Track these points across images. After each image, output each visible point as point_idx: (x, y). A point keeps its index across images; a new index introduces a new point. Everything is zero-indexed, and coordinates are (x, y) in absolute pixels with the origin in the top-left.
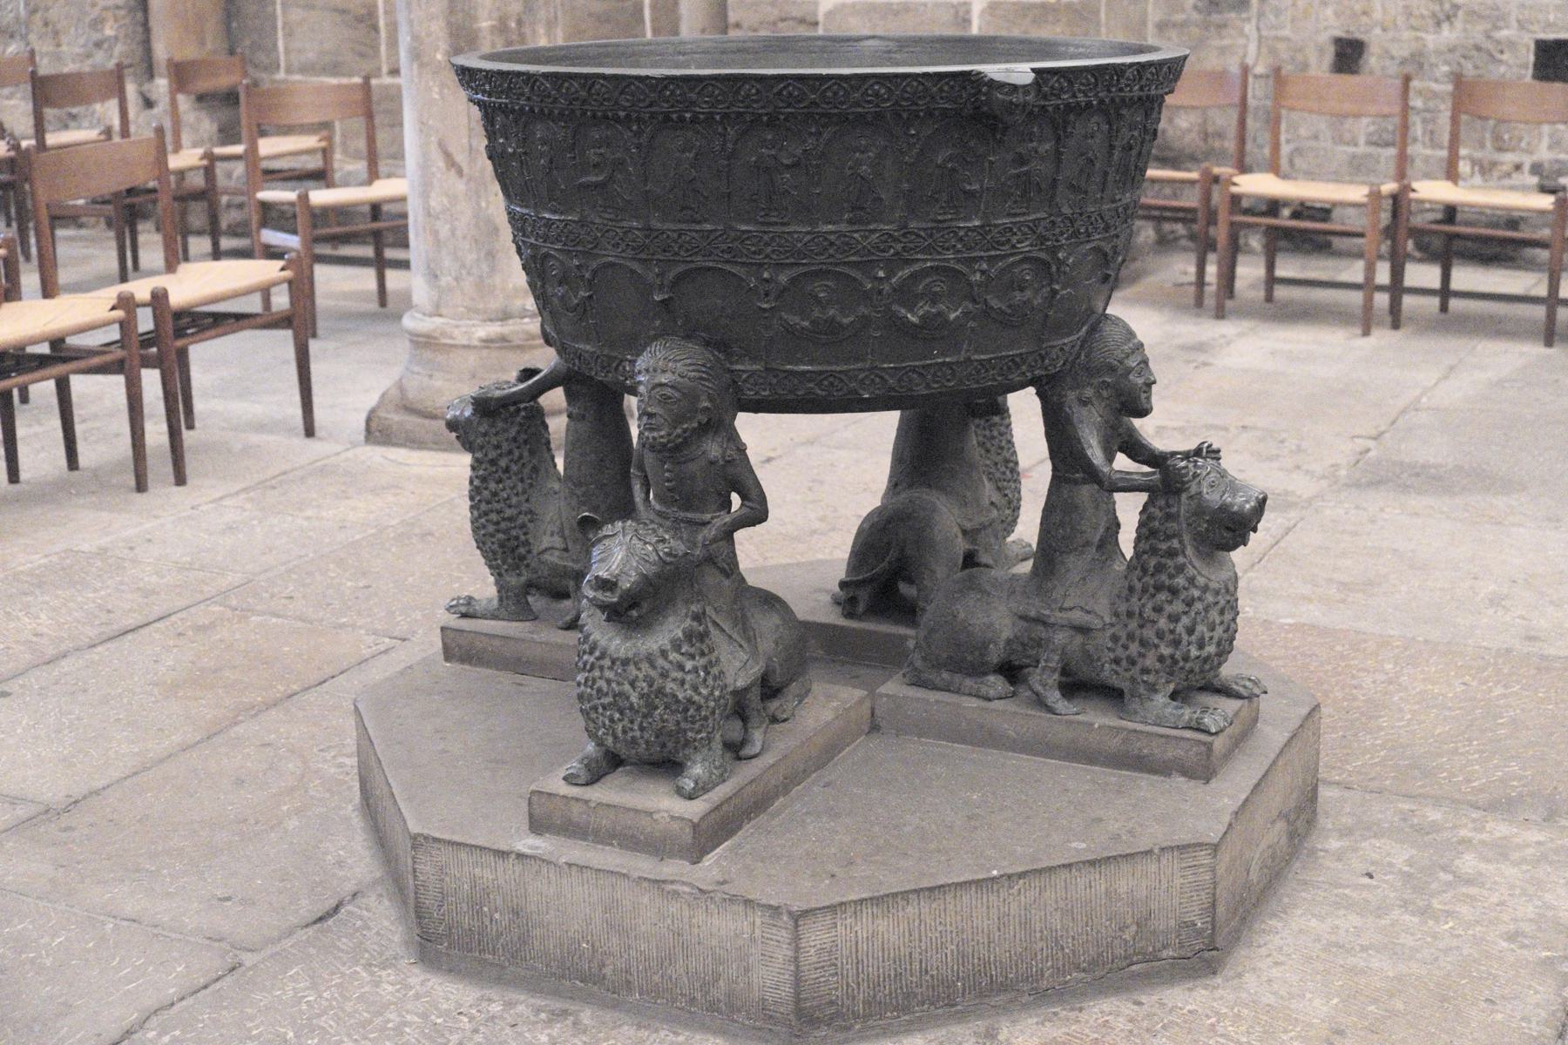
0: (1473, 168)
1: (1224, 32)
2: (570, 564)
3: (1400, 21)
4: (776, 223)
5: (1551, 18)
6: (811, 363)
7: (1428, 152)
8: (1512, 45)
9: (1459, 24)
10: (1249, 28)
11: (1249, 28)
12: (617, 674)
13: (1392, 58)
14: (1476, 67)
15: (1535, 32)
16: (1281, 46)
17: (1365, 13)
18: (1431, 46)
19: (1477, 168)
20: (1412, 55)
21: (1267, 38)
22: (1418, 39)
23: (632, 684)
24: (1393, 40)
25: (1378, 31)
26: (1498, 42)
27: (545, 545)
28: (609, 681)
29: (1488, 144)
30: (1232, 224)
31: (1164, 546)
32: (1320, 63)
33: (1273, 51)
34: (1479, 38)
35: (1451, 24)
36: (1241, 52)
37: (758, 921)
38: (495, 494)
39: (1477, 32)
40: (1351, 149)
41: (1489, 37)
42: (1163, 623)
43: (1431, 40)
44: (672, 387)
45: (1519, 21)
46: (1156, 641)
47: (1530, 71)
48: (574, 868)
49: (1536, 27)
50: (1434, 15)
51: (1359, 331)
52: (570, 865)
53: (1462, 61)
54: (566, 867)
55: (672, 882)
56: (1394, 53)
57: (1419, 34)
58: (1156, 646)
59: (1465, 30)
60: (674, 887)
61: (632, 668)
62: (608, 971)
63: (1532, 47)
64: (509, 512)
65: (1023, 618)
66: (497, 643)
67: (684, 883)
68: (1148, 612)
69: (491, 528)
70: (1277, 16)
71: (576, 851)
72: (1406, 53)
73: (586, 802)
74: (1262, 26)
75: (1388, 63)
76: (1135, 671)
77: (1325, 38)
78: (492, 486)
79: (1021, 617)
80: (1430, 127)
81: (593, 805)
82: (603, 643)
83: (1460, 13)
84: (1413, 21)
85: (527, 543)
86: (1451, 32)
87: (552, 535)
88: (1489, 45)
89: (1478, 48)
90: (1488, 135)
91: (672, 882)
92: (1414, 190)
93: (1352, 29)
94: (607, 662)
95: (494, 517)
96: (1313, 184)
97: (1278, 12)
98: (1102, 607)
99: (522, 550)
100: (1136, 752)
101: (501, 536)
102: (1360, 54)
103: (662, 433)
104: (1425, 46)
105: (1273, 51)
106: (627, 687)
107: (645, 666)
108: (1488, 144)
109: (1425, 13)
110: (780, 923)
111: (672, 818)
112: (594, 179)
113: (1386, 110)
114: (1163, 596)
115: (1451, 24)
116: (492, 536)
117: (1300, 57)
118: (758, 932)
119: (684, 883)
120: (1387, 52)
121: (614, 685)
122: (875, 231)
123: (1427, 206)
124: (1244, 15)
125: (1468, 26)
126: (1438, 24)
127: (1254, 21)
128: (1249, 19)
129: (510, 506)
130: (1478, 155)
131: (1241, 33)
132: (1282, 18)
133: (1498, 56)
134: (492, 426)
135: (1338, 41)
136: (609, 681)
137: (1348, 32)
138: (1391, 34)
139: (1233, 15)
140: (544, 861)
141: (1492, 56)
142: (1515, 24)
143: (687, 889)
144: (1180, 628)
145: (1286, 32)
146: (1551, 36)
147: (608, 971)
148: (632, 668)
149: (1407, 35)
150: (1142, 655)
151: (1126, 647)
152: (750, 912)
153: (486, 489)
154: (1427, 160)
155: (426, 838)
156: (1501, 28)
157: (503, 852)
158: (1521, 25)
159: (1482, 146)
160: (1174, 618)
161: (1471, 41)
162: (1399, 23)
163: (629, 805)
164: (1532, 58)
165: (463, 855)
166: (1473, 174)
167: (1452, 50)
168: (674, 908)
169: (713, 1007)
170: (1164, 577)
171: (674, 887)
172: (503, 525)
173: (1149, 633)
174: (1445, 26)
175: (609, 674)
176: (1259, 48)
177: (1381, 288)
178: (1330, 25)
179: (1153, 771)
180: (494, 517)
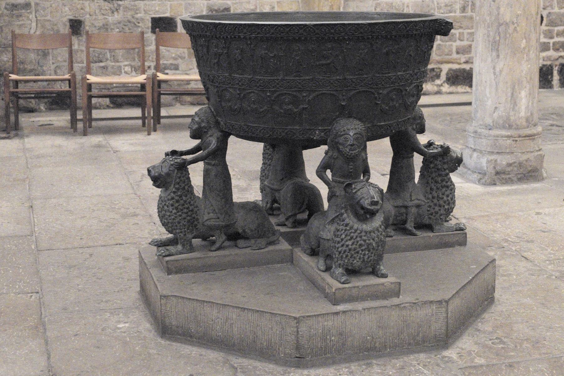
0: (132, 69)
1: (21, 19)
2: (221, 223)
3: (97, 11)
4: (387, 73)
5: (157, 9)
6: (385, 121)
7: (113, 64)
8: (142, 19)
9: (121, 12)
10: (32, 16)
11: (32, 16)
12: (367, 237)
13: (95, 27)
14: (129, 29)
15: (151, 15)
16: (47, 24)
17: (82, 9)
18: (111, 21)
19: (133, 69)
20: (103, 25)
21: (40, 20)
22: (105, 18)
23: (373, 240)
24: (95, 19)
25: (88, 16)
26: (137, 19)
27: (206, 218)
28: (365, 241)
29: (136, 59)
30: (145, 91)
31: (443, 173)
32: (65, 30)
33: (43, 26)
34: (130, 17)
35: (118, 12)
36: (29, 27)
37: (434, 308)
38: (185, 201)
39: (129, 15)
40: (80, 65)
41: (133, 17)
42: (445, 198)
43: (110, 19)
44: (360, 134)
45: (144, 10)
46: (444, 204)
47: (150, 30)
48: (366, 310)
49: (151, 13)
50: (111, 9)
51: (146, 133)
52: (364, 309)
53: (123, 27)
54: (363, 311)
55: (402, 304)
56: (97, 25)
57: (105, 16)
58: (444, 206)
59: (124, 15)
60: (404, 305)
61: (372, 234)
62: (377, 345)
63: (150, 20)
64: (191, 208)
65: (397, 207)
66: (194, 261)
67: (407, 303)
68: (441, 196)
69: (184, 215)
70: (44, 11)
71: (359, 306)
72: (101, 24)
73: (358, 287)
74: (37, 16)
75: (94, 29)
76: (437, 216)
77: (65, 19)
78: (184, 198)
79: (395, 207)
80: (113, 54)
81: (360, 287)
82: (360, 227)
83: (121, 8)
84: (103, 12)
85: (197, 220)
86: (118, 15)
87: (209, 213)
88: (133, 20)
89: (130, 22)
90: (136, 55)
91: (402, 304)
92: (88, 79)
93: (77, 16)
94: (363, 234)
95: (185, 210)
96: (108, 77)
97: (44, 9)
98: (421, 197)
99: (196, 223)
100: (444, 242)
101: (189, 218)
102: (81, 26)
103: (357, 151)
104: (108, 21)
105: (43, 26)
106: (372, 241)
107: (376, 232)
108: (136, 59)
109: (107, 8)
110: (442, 306)
111: (391, 283)
112: (324, 62)
113: (134, 46)
114: (444, 189)
115: (118, 12)
116: (184, 219)
117: (55, 28)
118: (434, 311)
119: (407, 303)
120: (93, 24)
121: (367, 241)
122: (408, 74)
123: (115, 85)
124: (29, 11)
125: (125, 13)
126: (113, 12)
127: (34, 13)
128: (31, 13)
129: (191, 205)
130: (133, 64)
131: (28, 19)
132: (46, 12)
133: (138, 24)
134: (182, 173)
135: (71, 20)
136: (365, 241)
137: (75, 17)
138: (94, 17)
139: (23, 11)
140: (354, 311)
141: (135, 24)
142: (143, 12)
143: (407, 305)
144: (449, 198)
145: (49, 18)
146: (157, 16)
147: (377, 345)
148: (372, 234)
149: (101, 17)
150: (440, 210)
151: (434, 209)
152: (432, 306)
153: (182, 200)
154: (113, 67)
155: (304, 317)
156: (137, 13)
157: (337, 313)
158: (145, 12)
159: (134, 60)
160: (448, 196)
161: (127, 19)
162: (97, 12)
163: (374, 283)
164: (150, 25)
165: (320, 319)
166: (132, 71)
167: (119, 23)
168: (404, 313)
169: (417, 344)
170: (444, 183)
171: (404, 305)
172: (189, 213)
173: (441, 202)
174: (116, 13)
175: (364, 238)
176: (37, 25)
177: (80, 120)
178: (68, 14)
179: (450, 247)
180: (185, 210)
